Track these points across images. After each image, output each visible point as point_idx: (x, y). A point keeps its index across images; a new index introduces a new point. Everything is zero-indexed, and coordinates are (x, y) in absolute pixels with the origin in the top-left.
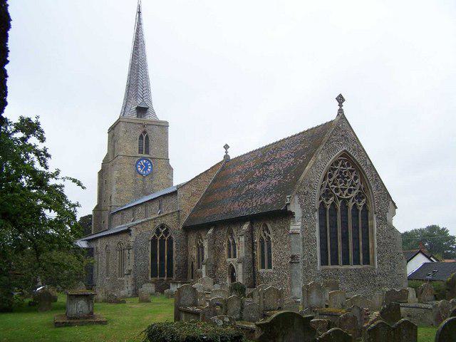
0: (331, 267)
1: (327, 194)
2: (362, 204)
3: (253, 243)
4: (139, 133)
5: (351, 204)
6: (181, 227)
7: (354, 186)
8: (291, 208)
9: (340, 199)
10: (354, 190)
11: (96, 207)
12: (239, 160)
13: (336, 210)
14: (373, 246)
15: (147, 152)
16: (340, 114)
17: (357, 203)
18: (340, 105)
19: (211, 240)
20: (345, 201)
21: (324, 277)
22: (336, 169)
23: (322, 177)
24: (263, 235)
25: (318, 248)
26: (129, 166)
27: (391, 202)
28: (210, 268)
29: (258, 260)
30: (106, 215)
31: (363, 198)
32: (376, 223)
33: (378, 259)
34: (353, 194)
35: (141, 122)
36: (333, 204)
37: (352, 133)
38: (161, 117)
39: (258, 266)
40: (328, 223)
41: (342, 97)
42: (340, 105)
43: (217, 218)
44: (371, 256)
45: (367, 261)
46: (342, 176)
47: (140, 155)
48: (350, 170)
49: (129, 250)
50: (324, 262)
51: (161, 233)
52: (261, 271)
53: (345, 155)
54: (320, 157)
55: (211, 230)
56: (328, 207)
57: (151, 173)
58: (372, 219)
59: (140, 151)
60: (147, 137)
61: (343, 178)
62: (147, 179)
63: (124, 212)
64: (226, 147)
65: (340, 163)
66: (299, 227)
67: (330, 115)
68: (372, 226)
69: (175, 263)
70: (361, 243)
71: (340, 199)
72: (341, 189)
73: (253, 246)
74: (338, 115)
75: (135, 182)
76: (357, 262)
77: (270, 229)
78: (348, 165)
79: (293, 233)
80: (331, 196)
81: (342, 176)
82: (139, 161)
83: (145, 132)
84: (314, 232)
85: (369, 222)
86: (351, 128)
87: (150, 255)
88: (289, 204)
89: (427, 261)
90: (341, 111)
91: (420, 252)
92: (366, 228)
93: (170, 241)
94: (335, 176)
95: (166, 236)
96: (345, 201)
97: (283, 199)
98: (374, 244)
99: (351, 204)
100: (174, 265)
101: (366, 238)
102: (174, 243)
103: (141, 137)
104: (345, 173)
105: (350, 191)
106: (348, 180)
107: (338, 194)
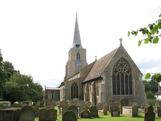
0: (117, 95)
1: (116, 71)
2: (129, 74)
3: (95, 88)
5: (125, 75)
6: (81, 83)
7: (126, 68)
9: (120, 73)
10: (126, 70)
11: (65, 77)
15: (79, 59)
18: (121, 42)
20: (122, 74)
22: (119, 63)
23: (114, 66)
25: (112, 89)
27: (140, 73)
28: (86, 96)
31: (130, 72)
32: (134, 81)
33: (135, 92)
34: (126, 71)
35: (77, 49)
36: (118, 74)
38: (84, 47)
39: (96, 95)
40: (116, 81)
42: (121, 42)
44: (133, 92)
45: (131, 93)
46: (121, 65)
48: (124, 63)
50: (114, 93)
52: (97, 96)
53: (122, 58)
56: (116, 76)
58: (133, 79)
59: (77, 59)
60: (79, 54)
64: (96, 57)
65: (121, 61)
67: (118, 46)
68: (133, 82)
70: (120, 88)
72: (121, 69)
75: (76, 69)
76: (127, 93)
78: (124, 61)
80: (117, 72)
81: (121, 65)
82: (77, 62)
83: (78, 53)
85: (132, 80)
87: (71, 92)
90: (121, 44)
92: (131, 82)
93: (77, 87)
94: (118, 65)
96: (122, 74)
99: (125, 75)
100: (79, 95)
102: (79, 88)
103: (77, 54)
104: (123, 64)
105: (125, 70)
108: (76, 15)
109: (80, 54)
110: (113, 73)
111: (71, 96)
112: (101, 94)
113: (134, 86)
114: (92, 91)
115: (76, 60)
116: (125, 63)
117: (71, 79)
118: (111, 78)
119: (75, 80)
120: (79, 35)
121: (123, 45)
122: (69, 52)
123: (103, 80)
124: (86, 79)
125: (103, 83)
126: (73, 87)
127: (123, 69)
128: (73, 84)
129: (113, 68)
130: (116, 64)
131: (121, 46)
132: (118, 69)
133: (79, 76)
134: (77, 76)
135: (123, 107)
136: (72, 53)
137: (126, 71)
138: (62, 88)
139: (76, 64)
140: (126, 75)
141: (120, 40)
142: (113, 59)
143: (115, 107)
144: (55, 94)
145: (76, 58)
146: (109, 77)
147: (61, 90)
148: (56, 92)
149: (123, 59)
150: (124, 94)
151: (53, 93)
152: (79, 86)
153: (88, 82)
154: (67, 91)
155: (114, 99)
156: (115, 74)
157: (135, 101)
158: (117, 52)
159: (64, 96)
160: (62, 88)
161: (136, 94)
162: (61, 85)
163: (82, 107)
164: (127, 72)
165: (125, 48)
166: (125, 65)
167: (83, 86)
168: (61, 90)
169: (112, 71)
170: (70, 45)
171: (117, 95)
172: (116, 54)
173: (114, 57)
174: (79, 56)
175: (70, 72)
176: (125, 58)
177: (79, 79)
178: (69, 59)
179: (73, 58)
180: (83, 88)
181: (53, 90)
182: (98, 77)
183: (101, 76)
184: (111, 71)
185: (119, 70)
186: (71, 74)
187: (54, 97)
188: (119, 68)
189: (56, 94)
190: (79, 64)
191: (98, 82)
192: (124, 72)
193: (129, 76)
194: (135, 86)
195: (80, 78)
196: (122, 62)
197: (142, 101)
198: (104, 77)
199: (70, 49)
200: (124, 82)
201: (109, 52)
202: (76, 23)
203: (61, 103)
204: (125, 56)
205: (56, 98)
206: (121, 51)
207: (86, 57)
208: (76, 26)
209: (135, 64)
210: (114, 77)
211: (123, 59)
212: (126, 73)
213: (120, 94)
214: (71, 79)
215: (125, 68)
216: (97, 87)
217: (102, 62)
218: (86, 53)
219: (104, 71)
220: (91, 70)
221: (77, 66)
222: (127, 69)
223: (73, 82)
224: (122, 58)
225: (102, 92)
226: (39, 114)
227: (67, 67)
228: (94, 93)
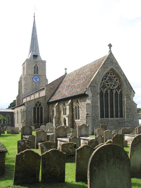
1: (104, 87)
2: (119, 91)
3: (73, 109)
4: (35, 65)
6: (46, 103)
7: (116, 83)
9: (109, 89)
11: (18, 96)
15: (37, 73)
18: (110, 48)
22: (108, 76)
23: (101, 79)
24: (76, 105)
25: (99, 111)
28: (57, 120)
29: (75, 116)
31: (120, 89)
34: (116, 87)
36: (106, 91)
38: (43, 59)
39: (75, 118)
41: (111, 45)
42: (110, 48)
44: (123, 114)
45: (121, 116)
46: (111, 79)
50: (102, 116)
51: (37, 105)
53: (112, 70)
56: (104, 93)
58: (124, 98)
59: (35, 73)
60: (37, 67)
64: (66, 69)
65: (110, 73)
67: (107, 54)
68: (124, 101)
69: (43, 117)
70: (119, 109)
72: (110, 85)
75: (32, 85)
76: (117, 116)
80: (105, 87)
81: (111, 79)
82: (34, 77)
83: (36, 65)
85: (123, 99)
86: (115, 59)
87: (33, 114)
90: (110, 51)
92: (121, 102)
93: (42, 108)
94: (107, 79)
96: (112, 90)
98: (125, 109)
99: (114, 92)
100: (43, 119)
102: (43, 109)
103: (35, 67)
104: (112, 78)
105: (114, 86)
107: (109, 87)
108: (34, 16)
110: (100, 89)
111: (33, 120)
112: (86, 116)
116: (115, 77)
117: (28, 99)
118: (99, 95)
119: (39, 99)
120: (37, 43)
121: (112, 53)
122: (24, 64)
123: (89, 98)
124: (54, 97)
125: (88, 101)
126: (40, 107)
127: (112, 85)
128: (36, 104)
130: (104, 78)
131: (111, 54)
132: (106, 84)
133: (43, 93)
136: (28, 65)
139: (33, 78)
140: (116, 92)
141: (109, 45)
142: (100, 71)
146: (96, 94)
147: (18, 113)
148: (8, 116)
149: (113, 70)
150: (113, 117)
152: (44, 107)
153: (59, 101)
154: (29, 113)
156: (103, 90)
157: (126, 126)
158: (105, 61)
159: (25, 119)
163: (100, 137)
164: (117, 88)
165: (115, 57)
167: (49, 106)
168: (18, 113)
169: (99, 86)
170: (26, 55)
172: (104, 63)
173: (102, 67)
175: (25, 89)
176: (116, 71)
177: (44, 98)
178: (24, 73)
179: (29, 72)
181: (3, 112)
183: (85, 92)
187: (5, 122)
189: (9, 118)
190: (36, 80)
191: (79, 101)
194: (126, 107)
195: (45, 96)
198: (90, 95)
199: (25, 60)
200: (113, 101)
201: (89, 63)
203: (57, 131)
205: (9, 123)
206: (110, 59)
208: (33, 31)
209: (126, 79)
210: (101, 94)
211: (113, 70)
212: (115, 90)
214: (28, 99)
215: (115, 83)
216: (76, 107)
217: (80, 75)
218: (45, 65)
219: (89, 86)
220: (61, 86)
221: (34, 81)
222: (118, 84)
223: (36, 102)
224: (112, 70)
225: (87, 114)
226: (77, 158)
227: (20, 83)
228: (70, 116)
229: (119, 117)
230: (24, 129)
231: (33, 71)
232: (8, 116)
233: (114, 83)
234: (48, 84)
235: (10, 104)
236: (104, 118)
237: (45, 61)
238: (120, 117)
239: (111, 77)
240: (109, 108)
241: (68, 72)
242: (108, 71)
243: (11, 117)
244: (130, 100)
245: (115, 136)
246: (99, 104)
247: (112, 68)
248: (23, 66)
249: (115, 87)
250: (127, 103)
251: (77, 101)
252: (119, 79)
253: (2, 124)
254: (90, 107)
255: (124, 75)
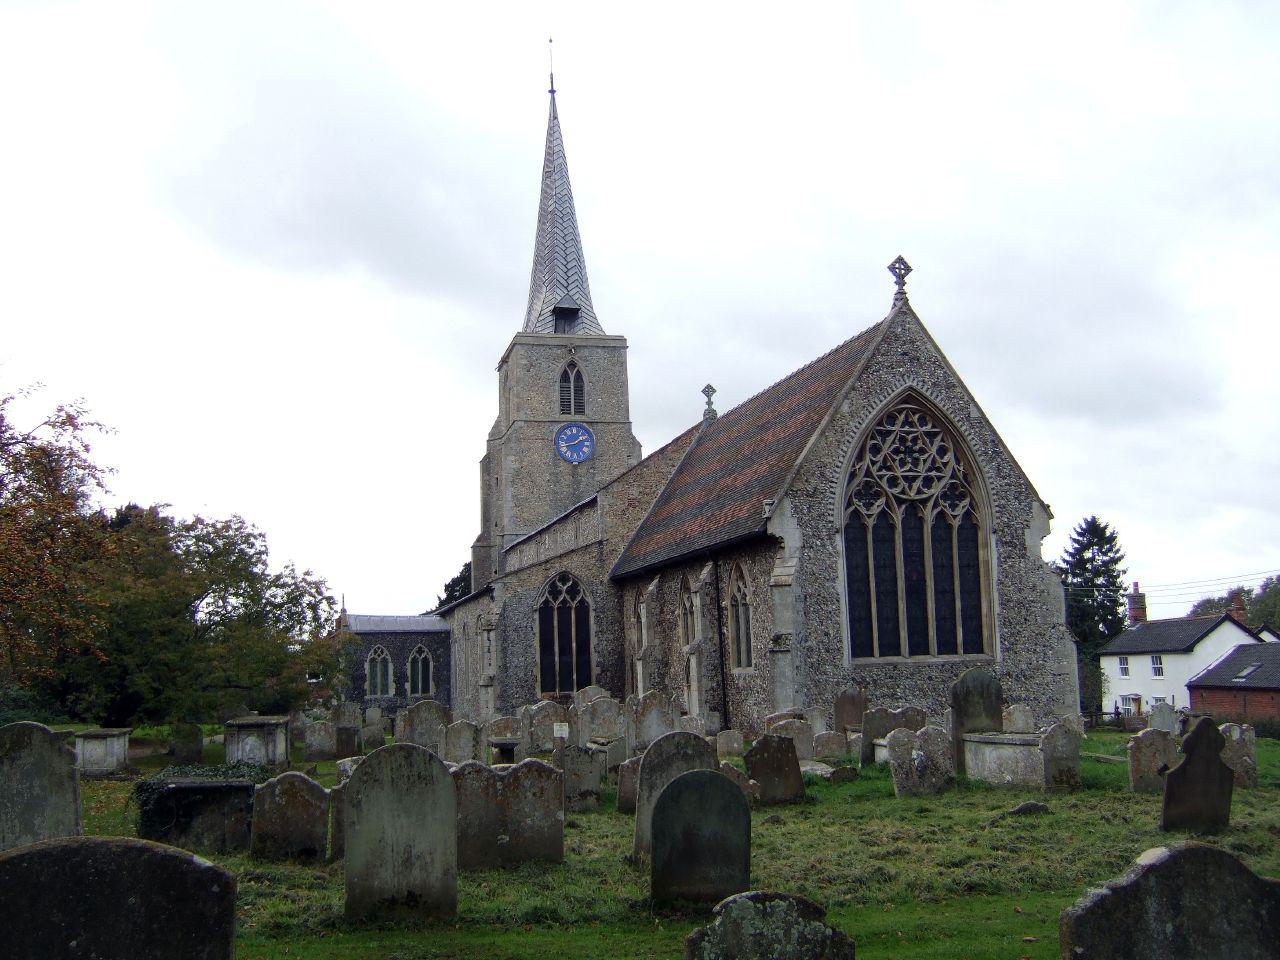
1: (868, 492)
2: (960, 511)
3: (720, 609)
4: (561, 366)
6: (606, 578)
7: (938, 469)
8: (773, 529)
9: (900, 502)
10: (939, 479)
11: (478, 540)
12: (735, 414)
13: (892, 527)
14: (990, 608)
15: (580, 409)
16: (899, 304)
17: (949, 511)
18: (901, 281)
19: (653, 604)
21: (859, 684)
22: (889, 433)
23: (851, 450)
24: (735, 590)
26: (539, 444)
28: (653, 668)
29: (731, 648)
30: (495, 554)
31: (962, 497)
32: (995, 556)
34: (936, 489)
36: (883, 515)
37: (929, 346)
41: (905, 263)
42: (901, 281)
43: (663, 556)
44: (985, 633)
45: (975, 644)
46: (907, 450)
47: (565, 417)
48: (927, 434)
49: (489, 631)
50: (861, 648)
51: (560, 592)
52: (736, 671)
53: (911, 397)
54: (845, 408)
55: (656, 581)
56: (870, 522)
57: (592, 458)
58: (986, 545)
59: (565, 408)
60: (579, 376)
61: (909, 451)
62: (582, 470)
63: (524, 547)
64: (709, 391)
65: (902, 418)
66: (793, 570)
67: (877, 309)
68: (987, 563)
69: (594, 658)
70: (958, 604)
71: (900, 502)
72: (906, 478)
73: (720, 617)
74: (894, 304)
76: (947, 646)
77: (746, 574)
78: (923, 421)
79: (777, 586)
80: (877, 495)
82: (561, 431)
83: (572, 365)
84: (834, 580)
85: (981, 552)
86: (930, 337)
87: (536, 643)
88: (769, 519)
89: (1245, 639)
90: (901, 297)
91: (1228, 618)
93: (583, 609)
94: (886, 449)
95: (555, 599)
96: (913, 508)
97: (759, 510)
98: (992, 604)
99: (929, 515)
100: (593, 664)
101: (973, 591)
102: (592, 615)
103: (565, 377)
105: (928, 482)
106: (922, 458)
107: (896, 491)
108: (552, 92)
109: (585, 379)
110: (849, 504)
111: (537, 672)
113: (996, 595)
114: (699, 636)
115: (558, 416)
116: (931, 436)
118: (840, 542)
127: (914, 478)
128: (553, 586)
129: (850, 469)
132: (881, 477)
134: (577, 530)
135: (967, 736)
137: (936, 489)
138: (465, 616)
139: (556, 443)
140: (941, 515)
141: (892, 268)
143: (925, 741)
144: (414, 661)
145: (557, 406)
148: (420, 651)
151: (399, 657)
152: (596, 602)
155: (862, 683)
156: (863, 511)
160: (471, 621)
161: (1008, 650)
162: (444, 596)
164: (944, 496)
166: (934, 450)
171: (881, 656)
174: (579, 390)
180: (621, 611)
182: (742, 532)
184: (838, 491)
185: (893, 482)
186: (525, 515)
187: (408, 686)
188: (889, 469)
192: (927, 492)
193: (956, 523)
196: (911, 424)
197: (1051, 699)
202: (548, 154)
204: (934, 384)
207: (625, 393)
209: (997, 441)
210: (854, 529)
212: (935, 505)
213: (898, 653)
222: (948, 472)
227: (488, 465)
229: (960, 650)
230: (417, 721)
231: (556, 396)
232: (420, 651)
233: (930, 470)
234: (645, 455)
235: (448, 588)
236: (872, 655)
237: (622, 339)
238: (882, 654)
239: (910, 437)
240: (902, 606)
241: (722, 407)
242: (887, 404)
243: (436, 659)
244: (1023, 556)
245: (754, 743)
246: (841, 586)
247: (911, 388)
248: (503, 370)
249: (933, 491)
250: (1005, 573)
251: (739, 569)
252: (956, 445)
253: (390, 700)
254: (790, 599)
255: (983, 421)
